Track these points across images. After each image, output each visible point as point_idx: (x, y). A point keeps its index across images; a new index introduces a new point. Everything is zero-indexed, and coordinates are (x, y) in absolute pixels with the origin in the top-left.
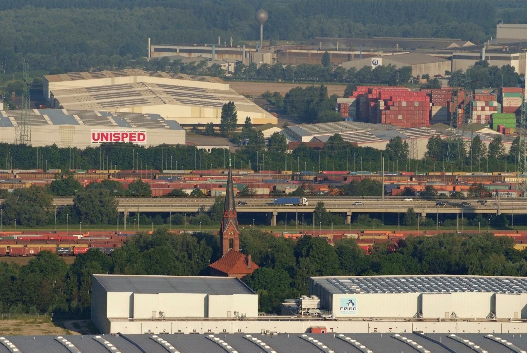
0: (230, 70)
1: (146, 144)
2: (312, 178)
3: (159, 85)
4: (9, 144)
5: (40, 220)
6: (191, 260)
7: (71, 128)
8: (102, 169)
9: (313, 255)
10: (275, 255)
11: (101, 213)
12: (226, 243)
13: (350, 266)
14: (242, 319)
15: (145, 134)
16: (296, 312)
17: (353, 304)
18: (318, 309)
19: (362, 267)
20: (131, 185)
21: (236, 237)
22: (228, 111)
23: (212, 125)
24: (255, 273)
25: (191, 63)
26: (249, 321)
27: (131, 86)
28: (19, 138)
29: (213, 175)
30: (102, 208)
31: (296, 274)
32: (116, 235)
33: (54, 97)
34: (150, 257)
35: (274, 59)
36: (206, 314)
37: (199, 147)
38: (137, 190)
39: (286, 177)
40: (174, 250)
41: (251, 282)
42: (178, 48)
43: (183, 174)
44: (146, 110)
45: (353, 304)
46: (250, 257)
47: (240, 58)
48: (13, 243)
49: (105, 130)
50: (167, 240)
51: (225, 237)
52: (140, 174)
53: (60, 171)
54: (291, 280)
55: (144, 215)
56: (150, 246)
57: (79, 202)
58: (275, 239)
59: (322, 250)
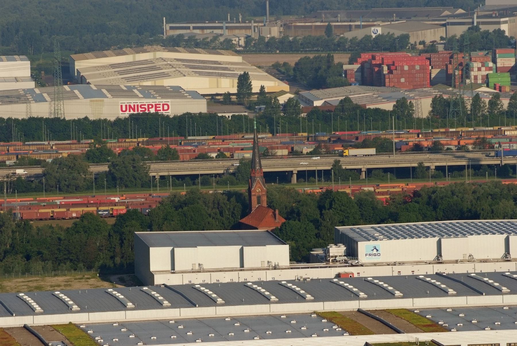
0: (240, 44)
1: (171, 113)
2: (326, 138)
3: (178, 60)
4: (45, 117)
5: (78, 187)
8: (131, 138)
11: (134, 177)
12: (254, 199)
13: (370, 216)
14: (275, 268)
16: (324, 259)
17: (377, 250)
18: (345, 256)
20: (160, 151)
22: (244, 81)
23: (229, 94)
25: (204, 39)
27: (151, 62)
28: (53, 111)
30: (136, 173)
32: (151, 197)
33: (81, 74)
34: (185, 215)
35: (280, 32)
37: (220, 115)
38: (166, 156)
40: (206, 208)
42: (191, 25)
44: (167, 82)
45: (377, 250)
46: (277, 212)
47: (249, 33)
48: (57, 208)
49: (132, 102)
50: (199, 199)
51: (253, 194)
52: (167, 141)
53: (93, 141)
54: (316, 231)
57: (114, 168)
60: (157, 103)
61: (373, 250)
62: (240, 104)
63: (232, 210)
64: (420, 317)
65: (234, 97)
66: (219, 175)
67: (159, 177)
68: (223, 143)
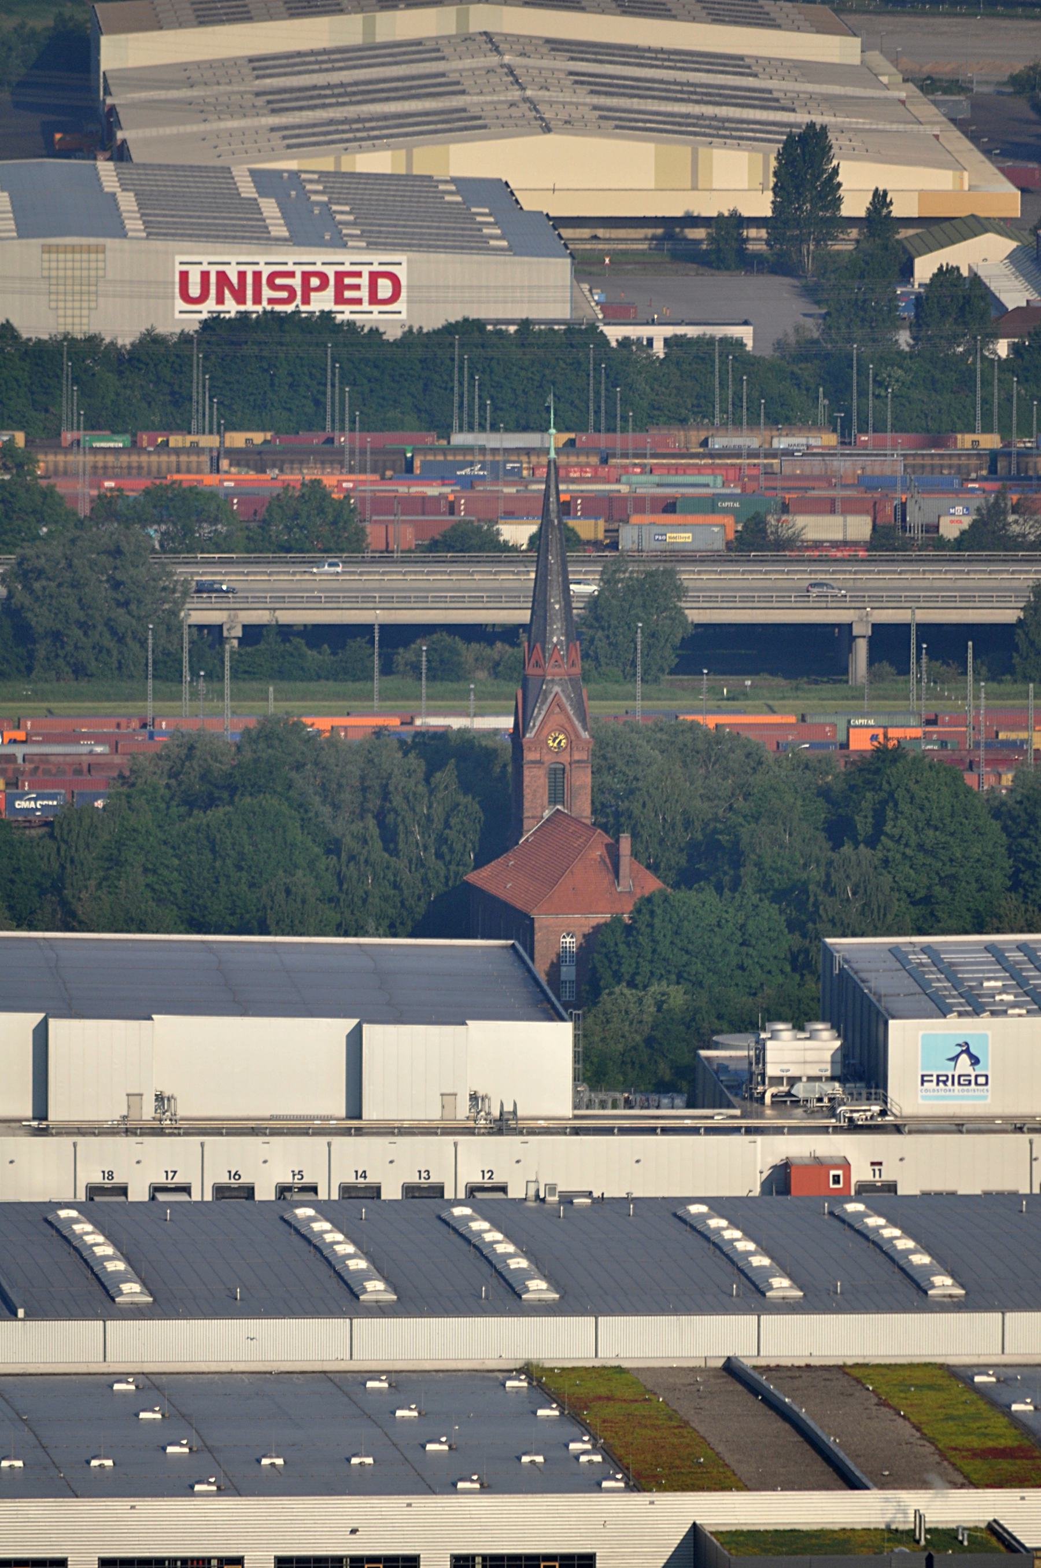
1: (393, 319)
3: (556, 45)
6: (394, 852)
7: (89, 250)
9: (896, 832)
10: (745, 833)
11: (113, 632)
12: (535, 783)
14: (504, 1125)
15: (401, 273)
16: (738, 1094)
17: (975, 1061)
18: (833, 1078)
21: (582, 756)
22: (804, 165)
24: (639, 911)
26: (533, 1132)
29: (654, 456)
30: (121, 611)
34: (212, 842)
36: (355, 1110)
39: (964, 461)
40: (327, 810)
41: (622, 949)
44: (468, 159)
45: (975, 1061)
49: (233, 260)
50: (299, 767)
51: (529, 756)
54: (794, 940)
55: (297, 640)
56: (225, 795)
57: (28, 588)
58: (760, 763)
60: (347, 268)
61: (955, 1059)
62: (779, 265)
63: (437, 825)
64: (981, 1405)
65: (756, 238)
67: (238, 632)
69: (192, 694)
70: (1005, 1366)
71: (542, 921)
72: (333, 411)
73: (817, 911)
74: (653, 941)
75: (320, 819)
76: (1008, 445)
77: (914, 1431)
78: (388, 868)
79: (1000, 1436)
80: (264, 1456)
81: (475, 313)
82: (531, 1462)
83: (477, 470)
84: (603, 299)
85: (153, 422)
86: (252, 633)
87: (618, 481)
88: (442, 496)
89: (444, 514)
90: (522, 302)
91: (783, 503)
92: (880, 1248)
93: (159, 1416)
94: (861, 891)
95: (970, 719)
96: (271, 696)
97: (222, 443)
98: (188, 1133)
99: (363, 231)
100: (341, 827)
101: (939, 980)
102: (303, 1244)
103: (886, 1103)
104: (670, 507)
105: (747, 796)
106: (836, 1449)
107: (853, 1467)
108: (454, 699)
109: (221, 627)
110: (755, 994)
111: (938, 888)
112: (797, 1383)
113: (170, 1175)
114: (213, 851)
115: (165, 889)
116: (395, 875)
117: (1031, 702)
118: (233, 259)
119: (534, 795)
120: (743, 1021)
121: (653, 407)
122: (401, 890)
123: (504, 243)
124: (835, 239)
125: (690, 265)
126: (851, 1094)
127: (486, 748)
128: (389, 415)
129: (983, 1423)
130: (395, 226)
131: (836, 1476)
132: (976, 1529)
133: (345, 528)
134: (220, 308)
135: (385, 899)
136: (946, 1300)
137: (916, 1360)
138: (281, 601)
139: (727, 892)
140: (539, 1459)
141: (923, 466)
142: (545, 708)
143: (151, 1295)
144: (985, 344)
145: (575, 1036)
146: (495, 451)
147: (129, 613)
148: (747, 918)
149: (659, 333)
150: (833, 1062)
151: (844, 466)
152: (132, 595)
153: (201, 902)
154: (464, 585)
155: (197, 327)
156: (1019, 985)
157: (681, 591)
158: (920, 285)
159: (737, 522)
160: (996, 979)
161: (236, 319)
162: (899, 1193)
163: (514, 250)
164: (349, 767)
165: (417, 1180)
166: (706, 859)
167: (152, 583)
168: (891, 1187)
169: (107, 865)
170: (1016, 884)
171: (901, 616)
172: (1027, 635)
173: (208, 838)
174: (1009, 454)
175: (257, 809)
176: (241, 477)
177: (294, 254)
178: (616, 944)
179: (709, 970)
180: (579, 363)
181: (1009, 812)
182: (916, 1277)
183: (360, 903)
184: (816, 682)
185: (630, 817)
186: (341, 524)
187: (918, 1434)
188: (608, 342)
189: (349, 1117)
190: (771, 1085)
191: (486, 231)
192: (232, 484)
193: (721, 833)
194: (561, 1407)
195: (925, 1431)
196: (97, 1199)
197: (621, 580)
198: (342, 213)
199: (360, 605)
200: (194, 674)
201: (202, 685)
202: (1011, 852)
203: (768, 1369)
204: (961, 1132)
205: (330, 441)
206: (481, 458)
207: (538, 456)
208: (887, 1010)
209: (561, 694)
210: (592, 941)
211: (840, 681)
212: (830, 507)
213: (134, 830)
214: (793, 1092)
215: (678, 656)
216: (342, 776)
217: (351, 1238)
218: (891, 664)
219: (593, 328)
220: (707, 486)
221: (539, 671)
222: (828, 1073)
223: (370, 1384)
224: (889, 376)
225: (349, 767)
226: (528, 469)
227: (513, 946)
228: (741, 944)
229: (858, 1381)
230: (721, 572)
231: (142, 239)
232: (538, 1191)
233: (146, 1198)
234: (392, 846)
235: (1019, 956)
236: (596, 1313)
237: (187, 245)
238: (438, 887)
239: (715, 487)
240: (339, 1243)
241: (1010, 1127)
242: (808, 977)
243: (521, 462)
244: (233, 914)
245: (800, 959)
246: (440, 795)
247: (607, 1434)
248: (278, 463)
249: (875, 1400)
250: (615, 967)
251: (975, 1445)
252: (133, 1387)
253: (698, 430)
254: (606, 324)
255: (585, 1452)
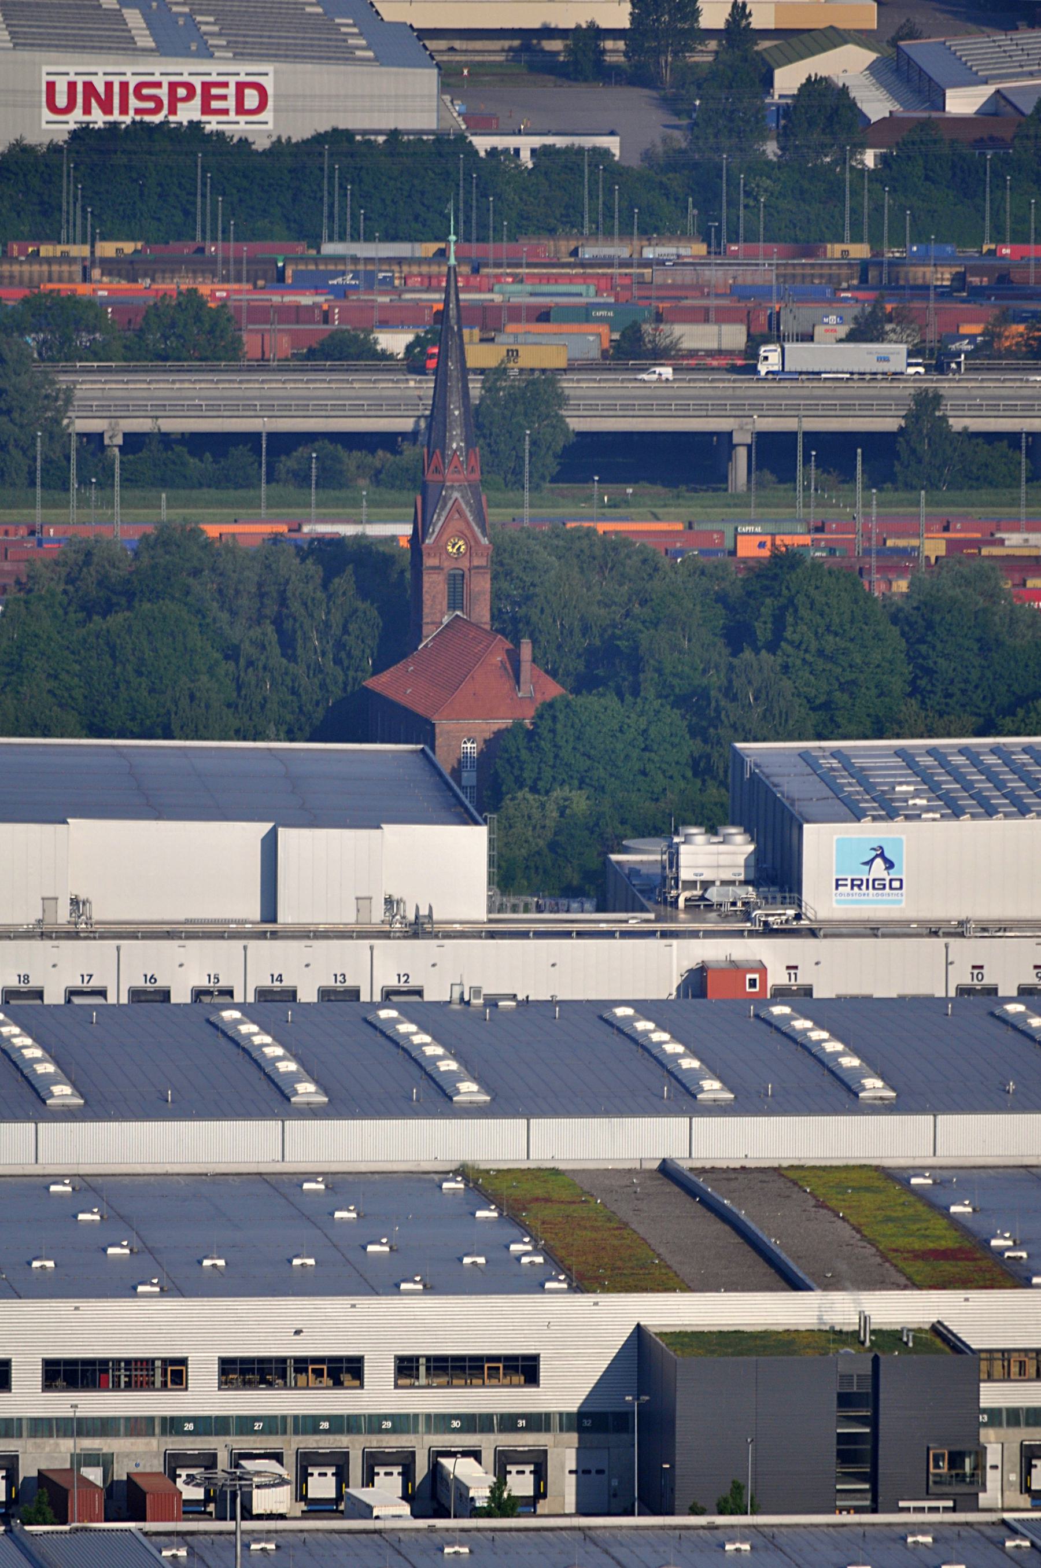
1: (261, 129)
2: (944, 277)
6: (293, 658)
9: (796, 637)
10: (644, 638)
12: (434, 588)
13: (966, 681)
14: (419, 929)
15: (268, 83)
16: (652, 899)
17: (890, 865)
18: (746, 882)
19: (1016, 688)
21: (476, 562)
23: (595, 33)
24: (541, 717)
29: (529, 265)
31: (715, 722)
34: (112, 648)
36: (270, 912)
39: (835, 271)
40: (225, 616)
41: (524, 754)
43: (400, 261)
46: (526, 650)
49: (101, 71)
50: (196, 573)
51: (429, 562)
55: (178, 448)
56: (123, 601)
58: (656, 569)
59: (837, 620)
60: (214, 78)
61: (869, 863)
62: (637, 76)
63: (336, 630)
64: (921, 1208)
66: (388, 441)
68: (476, 280)
69: (79, 501)
70: (941, 1168)
71: (443, 726)
72: (204, 221)
73: (718, 717)
74: (555, 746)
75: (218, 625)
76: (877, 253)
77: (854, 1233)
78: (286, 674)
79: (939, 1238)
80: (206, 1257)
81: (345, 122)
82: (474, 1263)
83: (349, 279)
84: (463, 109)
85: (22, 232)
86: (133, 442)
87: (491, 290)
88: (316, 306)
89: (318, 323)
90: (388, 111)
91: (657, 313)
92: (249, 1054)
93: (97, 1217)
94: (763, 696)
95: (859, 526)
96: (164, 503)
97: (92, 252)
98: (103, 937)
99: (229, 42)
100: (238, 633)
101: (850, 785)
102: (231, 1046)
103: (800, 906)
104: (544, 316)
105: (643, 603)
106: (778, 1251)
107: (795, 1269)
108: (337, 507)
109: (101, 435)
110: (657, 800)
111: (838, 694)
112: (734, 1185)
113: (86, 979)
114: (113, 656)
115: (66, 695)
116: (293, 681)
117: (923, 510)
118: (100, 70)
119: (433, 601)
120: (647, 826)
121: (522, 217)
122: (299, 696)
123: (370, 54)
124: (692, 50)
125: (547, 77)
126: (766, 898)
127: (384, 554)
128: (259, 224)
129: (924, 1225)
130: (261, 37)
131: (778, 1278)
132: (920, 1330)
133: (222, 338)
134: (87, 118)
135: (283, 704)
136: (877, 1102)
137: (852, 1162)
138: (162, 408)
139: (629, 698)
140: (481, 1260)
141: (794, 276)
142: (444, 514)
143: (82, 1096)
144: (853, 153)
145: (490, 841)
146: (368, 260)
147: (11, 421)
148: (650, 723)
149: (526, 144)
150: (746, 866)
151: (716, 275)
152: (14, 403)
153: (101, 707)
154: (343, 393)
155: (66, 137)
156: (931, 790)
157: (562, 399)
158: (781, 96)
159: (612, 331)
160: (908, 783)
161: (105, 129)
162: (815, 996)
163: (380, 60)
164: (247, 573)
165: (333, 983)
166: (605, 664)
167: (34, 391)
168: (808, 991)
169: (8, 670)
170: (914, 690)
171: (788, 424)
172: (908, 442)
173: (108, 644)
174: (881, 264)
175: (157, 614)
176: (115, 286)
177: (160, 64)
178: (518, 750)
179: (611, 775)
180: (448, 173)
181: (906, 618)
182: (846, 1079)
183: (258, 709)
184: (696, 491)
185: (528, 623)
186: (218, 333)
187: (858, 1236)
188: (477, 152)
189: (264, 921)
190: (684, 889)
191: (350, 41)
192: (106, 293)
193: (620, 638)
194: (499, 1208)
195: (866, 1233)
196: (12, 1002)
197: (503, 389)
198: (207, 23)
199: (241, 413)
200: (83, 482)
201: (93, 493)
202: (910, 659)
203: (703, 1171)
204: (876, 936)
205: (201, 250)
206: (352, 267)
207: (410, 265)
208: (800, 814)
209: (461, 500)
210: (493, 746)
211: (719, 489)
212: (703, 316)
213: (36, 636)
214: (707, 896)
215: (559, 464)
216: (240, 582)
217: (279, 1040)
218: (772, 472)
219: (461, 138)
220: (580, 295)
221: (438, 477)
222: (742, 878)
223: (307, 1186)
224: (758, 186)
225: (247, 573)
226: (400, 278)
227: (423, 750)
228: (643, 750)
229: (795, 1183)
230: (600, 381)
231: (8, 49)
232: (462, 993)
233: (62, 1001)
234: (290, 652)
235: (929, 761)
236: (528, 1115)
237: (54, 55)
238: (337, 692)
239: (587, 296)
240: (267, 1045)
241: (925, 931)
242: (710, 782)
243: (393, 272)
244: (133, 719)
245: (702, 765)
246: (339, 602)
247: (548, 1235)
248: (150, 273)
249: (813, 1202)
250: (517, 772)
251: (916, 1246)
252: (69, 1189)
253: (568, 240)
254: (473, 134)
255: (526, 1254)
